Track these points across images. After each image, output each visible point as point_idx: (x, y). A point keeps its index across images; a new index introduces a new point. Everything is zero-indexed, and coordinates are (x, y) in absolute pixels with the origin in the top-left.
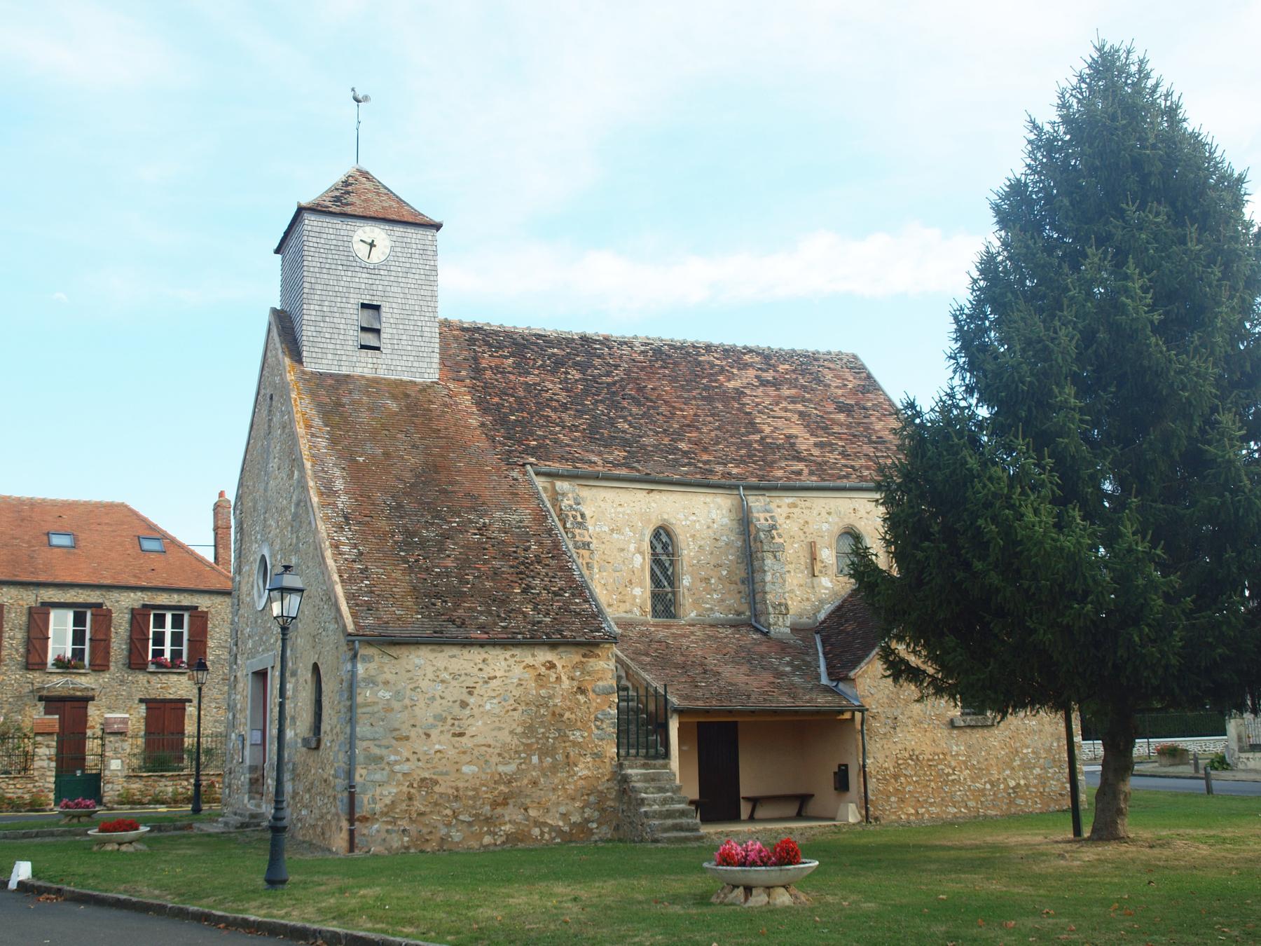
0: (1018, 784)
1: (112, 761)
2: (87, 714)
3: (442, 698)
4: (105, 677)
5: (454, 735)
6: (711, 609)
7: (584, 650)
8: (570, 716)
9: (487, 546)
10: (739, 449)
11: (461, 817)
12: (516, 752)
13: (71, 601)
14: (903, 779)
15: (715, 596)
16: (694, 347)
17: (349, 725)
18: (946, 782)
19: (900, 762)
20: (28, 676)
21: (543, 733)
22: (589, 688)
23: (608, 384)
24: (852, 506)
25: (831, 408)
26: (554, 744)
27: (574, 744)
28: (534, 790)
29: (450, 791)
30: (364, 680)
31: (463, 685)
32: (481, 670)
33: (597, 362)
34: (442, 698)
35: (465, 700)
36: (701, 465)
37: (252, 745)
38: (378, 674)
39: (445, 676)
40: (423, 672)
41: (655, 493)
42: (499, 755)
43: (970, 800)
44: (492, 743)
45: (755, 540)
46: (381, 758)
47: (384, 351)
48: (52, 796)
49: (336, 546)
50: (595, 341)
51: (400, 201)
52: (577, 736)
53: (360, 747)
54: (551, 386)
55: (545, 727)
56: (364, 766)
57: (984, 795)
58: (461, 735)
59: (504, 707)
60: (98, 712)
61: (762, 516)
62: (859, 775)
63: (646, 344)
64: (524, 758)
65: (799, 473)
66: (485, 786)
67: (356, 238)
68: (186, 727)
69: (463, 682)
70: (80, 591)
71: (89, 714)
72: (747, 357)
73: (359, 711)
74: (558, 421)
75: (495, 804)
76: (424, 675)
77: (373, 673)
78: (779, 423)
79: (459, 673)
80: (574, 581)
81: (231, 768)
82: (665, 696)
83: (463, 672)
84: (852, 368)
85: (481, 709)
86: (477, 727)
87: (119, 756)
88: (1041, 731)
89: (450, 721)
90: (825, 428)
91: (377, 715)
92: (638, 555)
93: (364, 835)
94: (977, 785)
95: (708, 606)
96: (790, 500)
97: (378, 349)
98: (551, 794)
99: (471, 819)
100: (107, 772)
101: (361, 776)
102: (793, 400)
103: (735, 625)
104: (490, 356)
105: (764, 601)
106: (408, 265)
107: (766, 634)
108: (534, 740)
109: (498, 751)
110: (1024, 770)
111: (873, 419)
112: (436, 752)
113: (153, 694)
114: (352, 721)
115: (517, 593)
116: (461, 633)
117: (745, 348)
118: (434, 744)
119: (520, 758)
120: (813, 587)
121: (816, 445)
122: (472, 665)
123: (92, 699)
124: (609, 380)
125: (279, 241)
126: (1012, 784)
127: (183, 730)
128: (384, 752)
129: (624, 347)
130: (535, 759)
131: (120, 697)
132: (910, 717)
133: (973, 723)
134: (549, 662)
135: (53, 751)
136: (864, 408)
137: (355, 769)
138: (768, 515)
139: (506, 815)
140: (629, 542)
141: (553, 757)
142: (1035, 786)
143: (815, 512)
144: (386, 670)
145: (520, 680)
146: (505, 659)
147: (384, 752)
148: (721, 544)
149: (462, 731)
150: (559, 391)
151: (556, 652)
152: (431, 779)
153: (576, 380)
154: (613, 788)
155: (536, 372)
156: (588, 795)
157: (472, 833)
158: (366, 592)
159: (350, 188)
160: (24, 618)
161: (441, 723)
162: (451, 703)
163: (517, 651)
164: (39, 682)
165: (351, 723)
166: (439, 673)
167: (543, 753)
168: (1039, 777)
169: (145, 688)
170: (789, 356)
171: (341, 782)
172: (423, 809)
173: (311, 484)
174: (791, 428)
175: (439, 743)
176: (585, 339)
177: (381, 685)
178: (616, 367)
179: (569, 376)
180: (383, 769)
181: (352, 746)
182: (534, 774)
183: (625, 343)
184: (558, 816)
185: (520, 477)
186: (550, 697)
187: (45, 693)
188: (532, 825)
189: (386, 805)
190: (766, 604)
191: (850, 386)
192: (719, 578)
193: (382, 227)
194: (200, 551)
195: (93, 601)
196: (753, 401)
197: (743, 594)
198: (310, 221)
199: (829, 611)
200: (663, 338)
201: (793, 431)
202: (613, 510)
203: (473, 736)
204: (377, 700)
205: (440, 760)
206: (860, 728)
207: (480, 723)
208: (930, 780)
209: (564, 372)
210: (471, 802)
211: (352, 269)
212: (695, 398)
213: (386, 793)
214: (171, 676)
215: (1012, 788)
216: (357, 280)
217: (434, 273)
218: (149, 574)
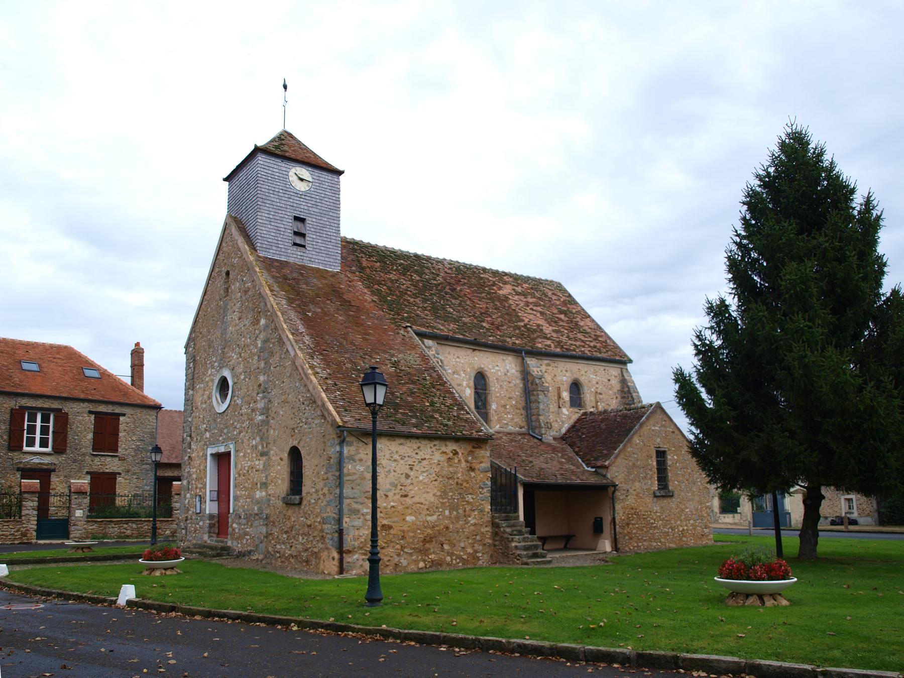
0: (683, 529)
1: (77, 511)
2: (50, 480)
3: (395, 471)
4: (62, 458)
5: (402, 496)
6: (507, 424)
7: (473, 444)
8: (466, 486)
9: (401, 375)
10: (515, 330)
11: (406, 550)
12: (437, 508)
14: (631, 526)
15: (509, 416)
16: (476, 268)
17: (338, 488)
18: (651, 528)
19: (630, 516)
20: (10, 454)
21: (452, 496)
22: (476, 467)
23: (435, 284)
24: (578, 367)
25: (556, 311)
26: (458, 503)
29: (399, 533)
30: (348, 458)
32: (417, 453)
33: (427, 271)
34: (395, 471)
35: (408, 473)
36: (498, 337)
37: (211, 500)
39: (396, 457)
40: (384, 454)
41: (477, 351)
42: (428, 509)
46: (358, 511)
47: (308, 248)
48: (34, 533)
49: (312, 367)
51: (315, 155)
52: (469, 498)
53: (346, 502)
54: (404, 282)
55: (452, 492)
56: (348, 516)
57: (668, 535)
58: (406, 496)
59: (430, 479)
60: (58, 479)
61: (535, 369)
63: (450, 264)
64: (441, 512)
65: (549, 346)
68: (117, 490)
69: (407, 461)
70: (46, 400)
71: (52, 480)
72: (505, 278)
73: (346, 478)
74: (414, 303)
76: (384, 456)
77: (352, 453)
78: (531, 317)
81: (187, 517)
82: (515, 474)
84: (560, 290)
85: (417, 480)
86: (415, 491)
89: (399, 487)
90: (556, 322)
91: (356, 482)
94: (666, 529)
95: (505, 422)
96: (546, 362)
97: (304, 246)
98: (456, 535)
99: (412, 551)
100: (73, 518)
101: (346, 522)
102: (536, 305)
104: (366, 260)
105: (538, 420)
107: (540, 440)
108: (446, 500)
110: (686, 521)
111: (578, 319)
112: (391, 507)
113: (95, 468)
114: (340, 485)
115: (428, 406)
116: (404, 429)
117: (503, 272)
119: (439, 512)
122: (412, 450)
123: (54, 470)
124: (435, 282)
126: (681, 529)
127: (115, 492)
128: (360, 507)
129: (439, 264)
130: (447, 512)
131: (73, 470)
133: (664, 494)
134: (455, 450)
135: (36, 504)
138: (539, 369)
141: (457, 511)
142: (691, 531)
143: (559, 371)
145: (439, 461)
146: (431, 448)
148: (512, 385)
150: (409, 286)
151: (458, 444)
153: (418, 281)
154: (488, 531)
155: (394, 273)
160: (8, 416)
161: (394, 488)
162: (400, 475)
163: (437, 443)
164: (17, 459)
165: (340, 487)
166: (393, 454)
167: (451, 509)
168: (692, 525)
170: (527, 279)
172: (384, 545)
173: (285, 326)
174: (537, 320)
175: (393, 501)
176: (417, 257)
177: (358, 462)
179: (413, 278)
180: (359, 518)
181: (341, 503)
182: (446, 522)
183: (439, 262)
184: (460, 549)
185: (405, 334)
186: (455, 473)
187: (22, 466)
188: (446, 555)
189: (361, 542)
190: (539, 422)
194: (123, 379)
197: (523, 416)
198: (261, 158)
199: (567, 428)
200: (460, 261)
202: (454, 360)
204: (355, 472)
205: (393, 512)
207: (416, 488)
208: (644, 527)
213: (361, 534)
214: (107, 457)
215: (681, 531)
216: (291, 201)
217: (338, 203)
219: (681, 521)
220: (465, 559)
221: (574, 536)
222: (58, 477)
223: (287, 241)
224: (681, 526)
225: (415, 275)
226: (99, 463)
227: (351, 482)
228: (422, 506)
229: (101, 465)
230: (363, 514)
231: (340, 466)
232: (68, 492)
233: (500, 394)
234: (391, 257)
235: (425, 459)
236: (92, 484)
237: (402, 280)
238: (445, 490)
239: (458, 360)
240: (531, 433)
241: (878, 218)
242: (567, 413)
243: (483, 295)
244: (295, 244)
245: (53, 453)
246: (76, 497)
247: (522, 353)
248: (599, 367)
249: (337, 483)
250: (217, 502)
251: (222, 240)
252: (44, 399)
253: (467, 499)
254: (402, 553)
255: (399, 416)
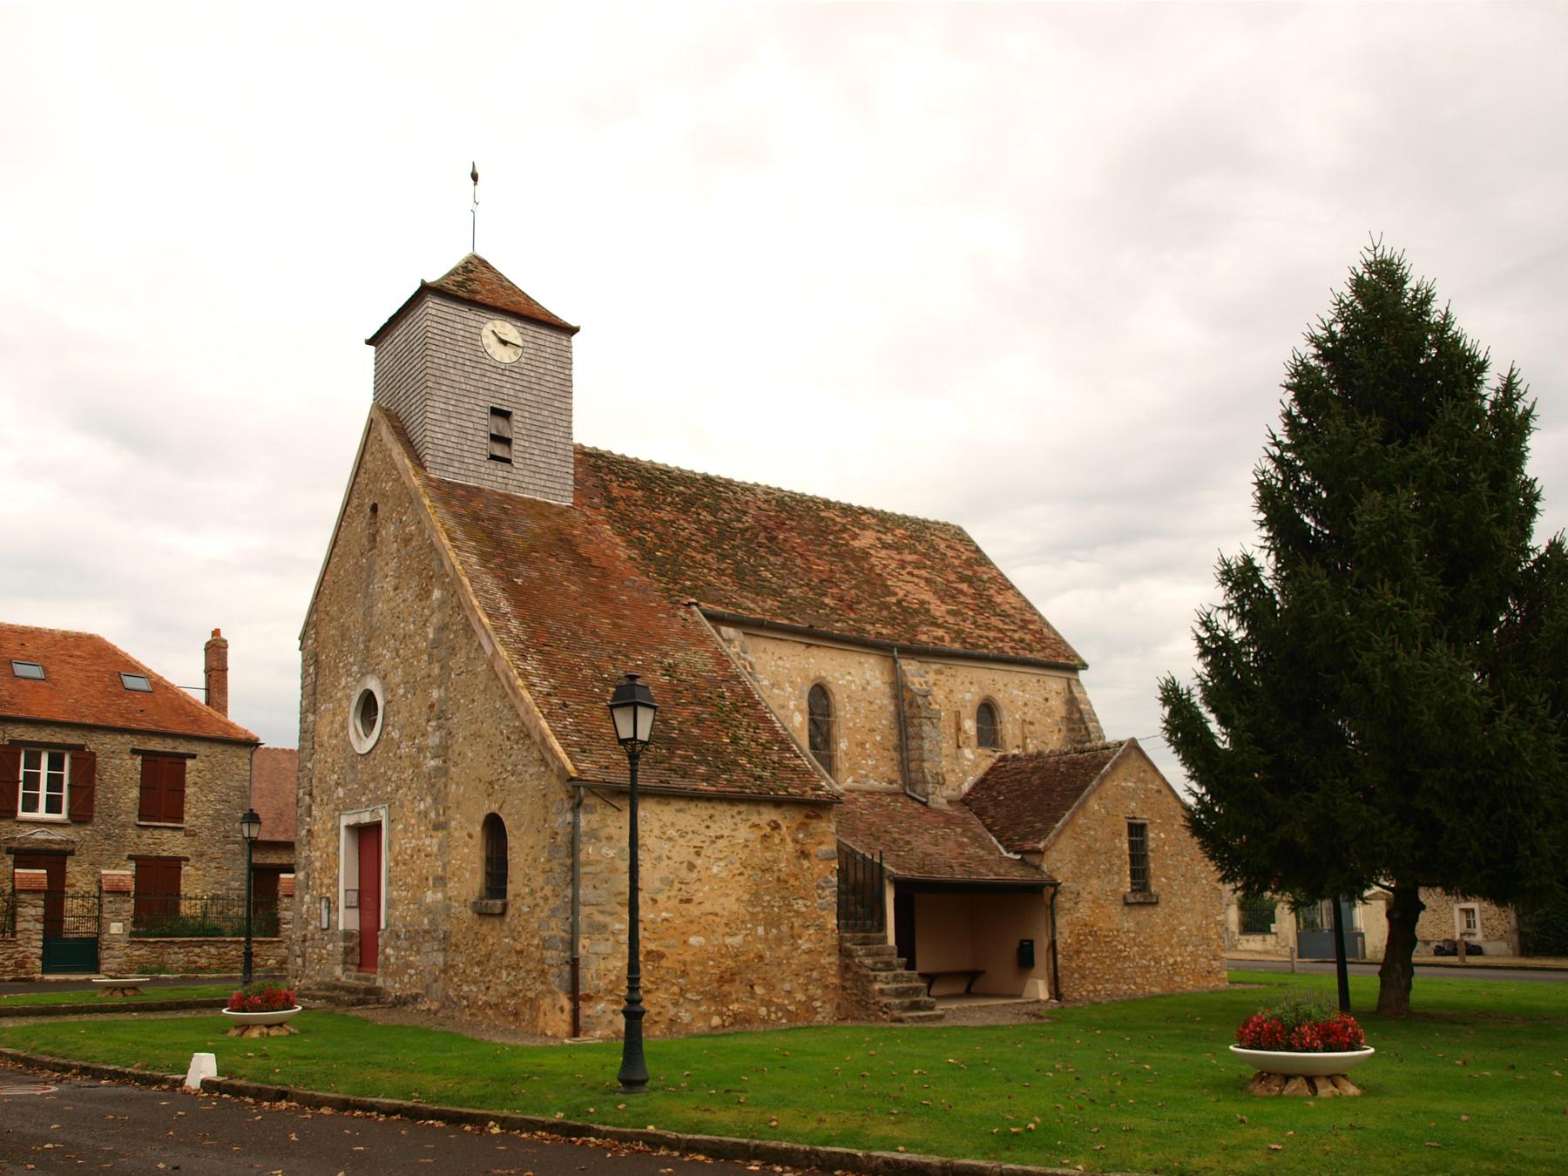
0: (1176, 961)
1: (112, 924)
3: (669, 858)
4: (85, 831)
5: (682, 901)
6: (866, 776)
7: (808, 811)
9: (680, 689)
10: (880, 610)
11: (689, 995)
13: (46, 740)
14: (1083, 955)
15: (870, 762)
17: (570, 886)
18: (1118, 959)
19: (1082, 938)
21: (769, 901)
23: (740, 529)
25: (953, 577)
27: (798, 913)
28: (760, 964)
29: (677, 966)
30: (586, 834)
31: (691, 844)
32: (708, 827)
33: (725, 506)
34: (669, 858)
36: (851, 623)
37: (347, 907)
38: (601, 828)
39: (672, 832)
40: (650, 828)
42: (727, 925)
43: (1138, 977)
44: (718, 909)
45: (911, 705)
46: (605, 926)
47: (516, 465)
49: (524, 675)
50: (719, 484)
51: (528, 298)
52: (800, 905)
54: (686, 525)
55: (770, 894)
57: (1149, 972)
58: (689, 901)
60: (79, 869)
61: (916, 680)
62: (1048, 950)
63: (767, 493)
64: (751, 929)
65: (942, 639)
66: (713, 960)
67: (486, 331)
68: (182, 888)
71: (68, 870)
72: (863, 518)
73: (583, 870)
74: (703, 562)
75: (722, 980)
77: (595, 826)
78: (910, 587)
79: (685, 830)
80: (777, 733)
81: (305, 936)
83: (690, 829)
85: (708, 873)
87: (121, 918)
88: (1193, 909)
89: (676, 885)
92: (797, 713)
93: (589, 1016)
94: (1144, 962)
95: (863, 772)
97: (508, 461)
99: (699, 998)
100: (106, 936)
101: (584, 947)
103: (893, 794)
106: (542, 371)
107: (925, 804)
108: (759, 909)
109: (724, 921)
110: (1180, 947)
112: (663, 920)
113: (143, 850)
114: (574, 882)
118: (661, 911)
119: (746, 929)
120: (957, 758)
121: (949, 612)
123: (72, 853)
124: (740, 525)
125: (378, 329)
126: (1171, 961)
128: (607, 919)
130: (761, 930)
132: (1090, 893)
133: (1142, 900)
134: (775, 822)
135: (41, 911)
136: (981, 580)
137: (578, 941)
138: (922, 680)
139: (733, 992)
140: (789, 699)
141: (778, 927)
144: (609, 823)
145: (747, 840)
146: (733, 817)
147: (607, 919)
148: (875, 707)
149: (689, 896)
150: (694, 532)
151: (780, 811)
152: (657, 952)
156: (811, 970)
157: (700, 1013)
158: (572, 731)
159: (471, 275)
161: (668, 888)
163: (743, 808)
165: (573, 884)
166: (665, 829)
167: (769, 924)
169: (135, 843)
171: (554, 956)
173: (476, 602)
175: (667, 910)
176: (708, 480)
177: (604, 841)
178: (745, 513)
180: (607, 940)
181: (574, 913)
183: (748, 489)
185: (688, 617)
186: (774, 862)
187: (15, 845)
188: (758, 1003)
189: (611, 982)
190: (923, 772)
191: (964, 558)
192: (874, 744)
193: (514, 323)
194: (191, 693)
195: (73, 742)
196: (818, 577)
197: (895, 762)
198: (432, 305)
201: (922, 597)
203: (700, 903)
204: (600, 858)
205: (667, 930)
206: (1049, 903)
207: (707, 888)
209: (694, 513)
210: (698, 978)
211: (481, 366)
212: (826, 554)
214: (164, 831)
215: (1172, 965)
217: (568, 383)
218: (138, 715)
219: (1172, 947)
220: (792, 1012)
221: (983, 972)
222: (79, 864)
223: (479, 451)
224: (1172, 956)
225: (705, 513)
226: (150, 841)
227: (591, 876)
228: (717, 919)
229: (155, 844)
230: (613, 933)
231: (573, 848)
232: (97, 890)
233: (855, 724)
234: (662, 480)
235: (722, 837)
236: (138, 877)
237: (681, 522)
238: (757, 891)
239: (780, 663)
240: (909, 792)
241: (1528, 414)
242: (972, 757)
243: (825, 548)
244: (493, 457)
245: (69, 822)
246: (111, 899)
247: (892, 652)
248: (1028, 676)
249: (568, 879)
250: (357, 910)
251: (364, 449)
252: (53, 728)
253: (796, 907)
254: (682, 1000)
255: (677, 761)
